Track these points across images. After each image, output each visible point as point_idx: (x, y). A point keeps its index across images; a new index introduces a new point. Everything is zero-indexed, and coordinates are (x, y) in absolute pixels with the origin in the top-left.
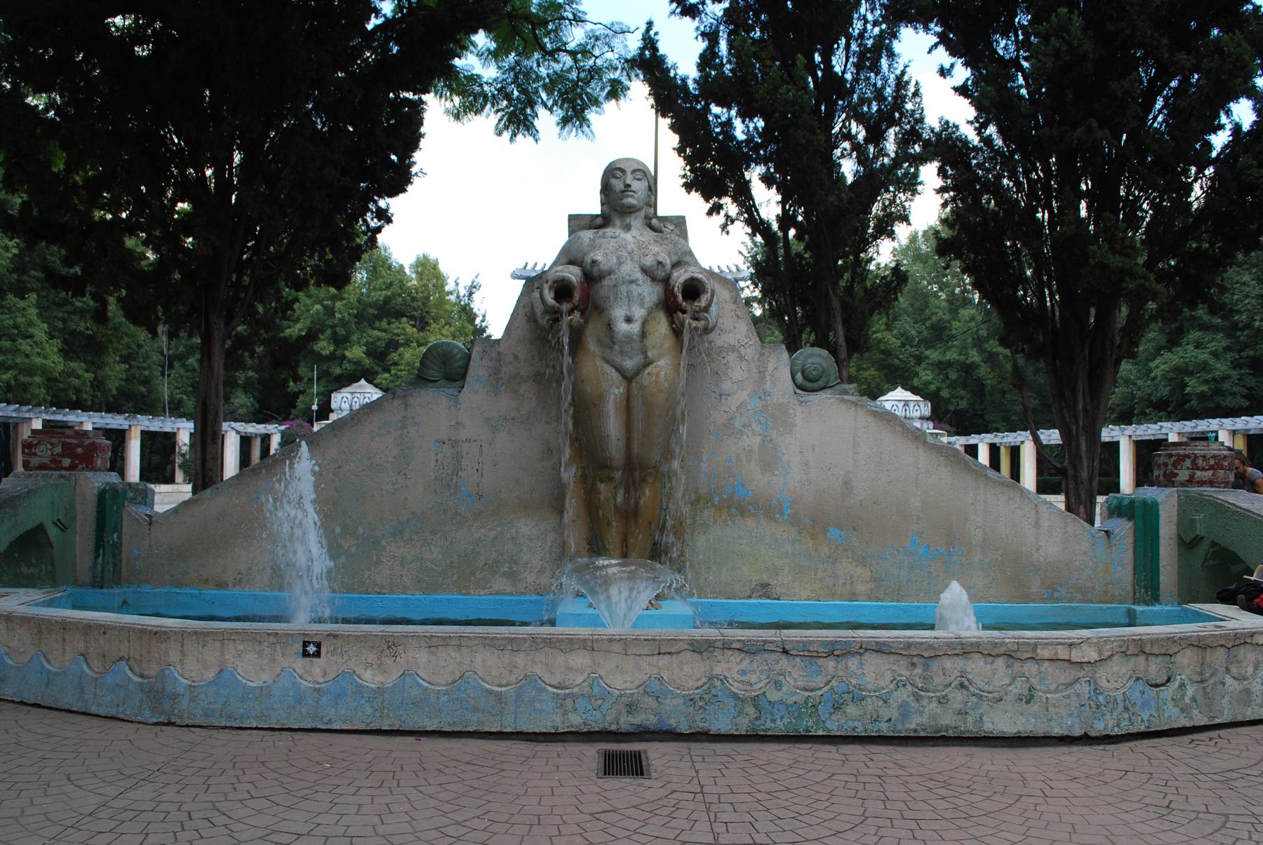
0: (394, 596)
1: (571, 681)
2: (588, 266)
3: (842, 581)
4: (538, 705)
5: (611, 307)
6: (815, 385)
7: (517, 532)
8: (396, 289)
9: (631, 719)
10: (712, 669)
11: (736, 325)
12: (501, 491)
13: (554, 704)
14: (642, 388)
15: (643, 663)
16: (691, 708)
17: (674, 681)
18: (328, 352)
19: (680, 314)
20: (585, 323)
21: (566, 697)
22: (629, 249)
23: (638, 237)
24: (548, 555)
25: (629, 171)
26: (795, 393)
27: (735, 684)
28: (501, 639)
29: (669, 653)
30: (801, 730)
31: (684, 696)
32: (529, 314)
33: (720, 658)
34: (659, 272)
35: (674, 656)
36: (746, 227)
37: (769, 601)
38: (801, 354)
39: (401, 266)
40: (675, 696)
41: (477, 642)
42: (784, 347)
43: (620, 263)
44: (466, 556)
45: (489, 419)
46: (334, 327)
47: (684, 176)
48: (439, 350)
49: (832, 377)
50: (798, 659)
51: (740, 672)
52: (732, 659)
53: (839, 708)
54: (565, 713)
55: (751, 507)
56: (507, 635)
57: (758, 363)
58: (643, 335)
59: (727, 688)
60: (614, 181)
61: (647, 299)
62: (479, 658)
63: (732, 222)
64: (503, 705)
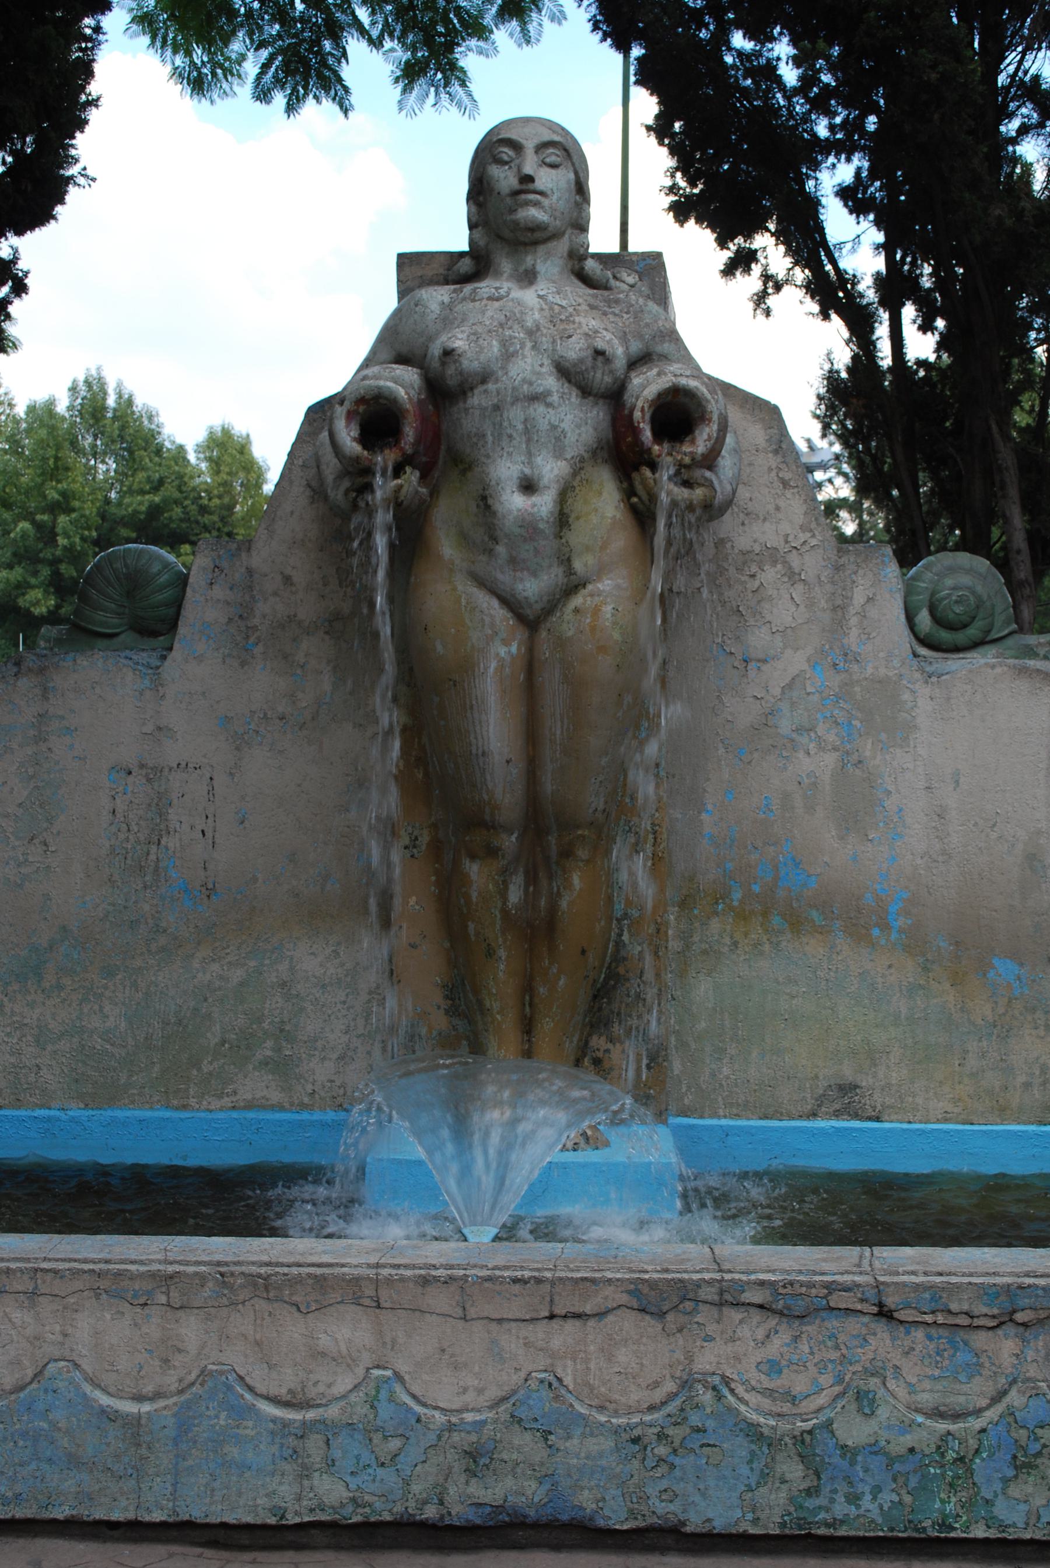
0: (22, 1113)
1: (321, 1388)
2: (436, 364)
3: (1021, 1079)
4: (233, 1452)
5: (488, 456)
6: (960, 637)
7: (292, 969)
8: (170, 491)
9: (477, 1491)
10: (690, 1358)
11: (782, 503)
12: (255, 879)
13: (275, 1449)
14: (561, 643)
15: (511, 1340)
16: (636, 1463)
17: (592, 1388)
18: (44, 610)
19: (648, 473)
20: (431, 495)
21: (306, 1430)
22: (529, 324)
23: (550, 298)
24: (361, 1022)
25: (529, 146)
26: (915, 655)
27: (752, 1398)
28: (141, 1276)
29: (578, 1316)
30: (927, 1523)
31: (616, 1431)
32: (314, 484)
33: (711, 1328)
34: (599, 375)
35: (591, 1323)
36: (808, 299)
37: (856, 1124)
38: (927, 567)
39: (181, 449)
40: (591, 1429)
41: (78, 1285)
42: (888, 550)
43: (508, 356)
44: (180, 1023)
45: (228, 719)
46: (55, 562)
47: (673, 189)
48: (118, 565)
49: (999, 620)
50: (919, 1334)
51: (764, 1367)
52: (744, 1332)
53: (1030, 1466)
54: (305, 1473)
55: (814, 914)
56: (155, 1267)
57: (829, 588)
58: (563, 520)
59: (730, 1409)
60: (495, 171)
61: (571, 437)
62: (84, 1325)
63: (778, 287)
64: (144, 1451)
